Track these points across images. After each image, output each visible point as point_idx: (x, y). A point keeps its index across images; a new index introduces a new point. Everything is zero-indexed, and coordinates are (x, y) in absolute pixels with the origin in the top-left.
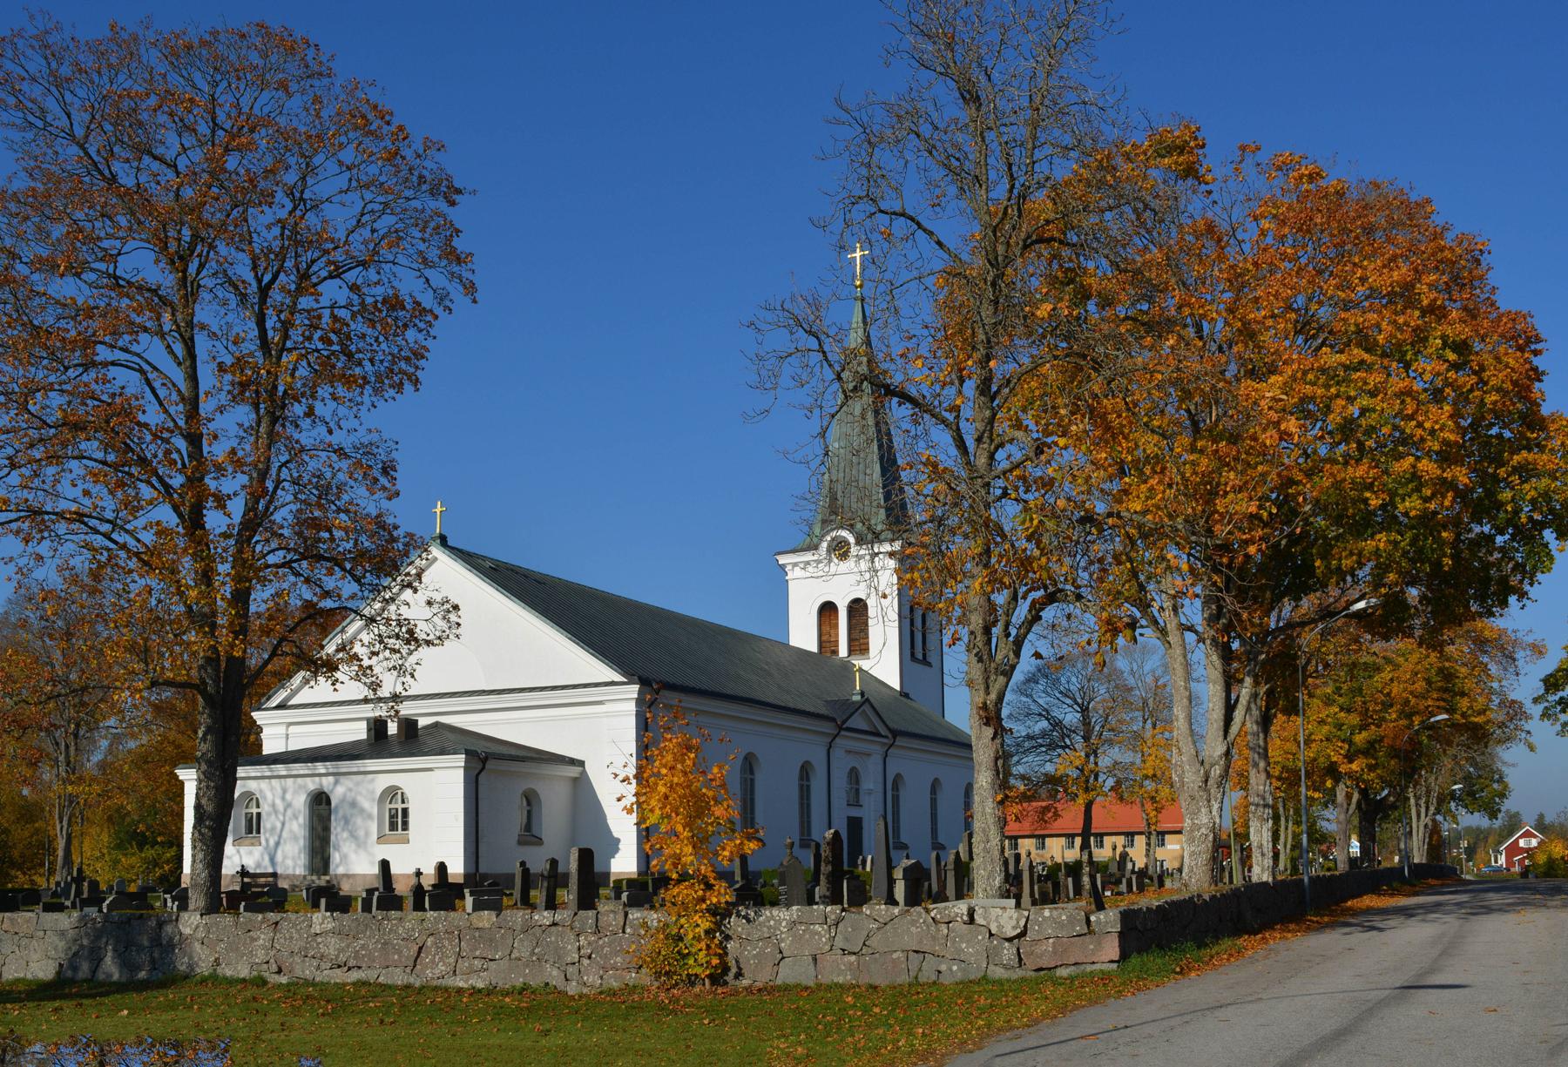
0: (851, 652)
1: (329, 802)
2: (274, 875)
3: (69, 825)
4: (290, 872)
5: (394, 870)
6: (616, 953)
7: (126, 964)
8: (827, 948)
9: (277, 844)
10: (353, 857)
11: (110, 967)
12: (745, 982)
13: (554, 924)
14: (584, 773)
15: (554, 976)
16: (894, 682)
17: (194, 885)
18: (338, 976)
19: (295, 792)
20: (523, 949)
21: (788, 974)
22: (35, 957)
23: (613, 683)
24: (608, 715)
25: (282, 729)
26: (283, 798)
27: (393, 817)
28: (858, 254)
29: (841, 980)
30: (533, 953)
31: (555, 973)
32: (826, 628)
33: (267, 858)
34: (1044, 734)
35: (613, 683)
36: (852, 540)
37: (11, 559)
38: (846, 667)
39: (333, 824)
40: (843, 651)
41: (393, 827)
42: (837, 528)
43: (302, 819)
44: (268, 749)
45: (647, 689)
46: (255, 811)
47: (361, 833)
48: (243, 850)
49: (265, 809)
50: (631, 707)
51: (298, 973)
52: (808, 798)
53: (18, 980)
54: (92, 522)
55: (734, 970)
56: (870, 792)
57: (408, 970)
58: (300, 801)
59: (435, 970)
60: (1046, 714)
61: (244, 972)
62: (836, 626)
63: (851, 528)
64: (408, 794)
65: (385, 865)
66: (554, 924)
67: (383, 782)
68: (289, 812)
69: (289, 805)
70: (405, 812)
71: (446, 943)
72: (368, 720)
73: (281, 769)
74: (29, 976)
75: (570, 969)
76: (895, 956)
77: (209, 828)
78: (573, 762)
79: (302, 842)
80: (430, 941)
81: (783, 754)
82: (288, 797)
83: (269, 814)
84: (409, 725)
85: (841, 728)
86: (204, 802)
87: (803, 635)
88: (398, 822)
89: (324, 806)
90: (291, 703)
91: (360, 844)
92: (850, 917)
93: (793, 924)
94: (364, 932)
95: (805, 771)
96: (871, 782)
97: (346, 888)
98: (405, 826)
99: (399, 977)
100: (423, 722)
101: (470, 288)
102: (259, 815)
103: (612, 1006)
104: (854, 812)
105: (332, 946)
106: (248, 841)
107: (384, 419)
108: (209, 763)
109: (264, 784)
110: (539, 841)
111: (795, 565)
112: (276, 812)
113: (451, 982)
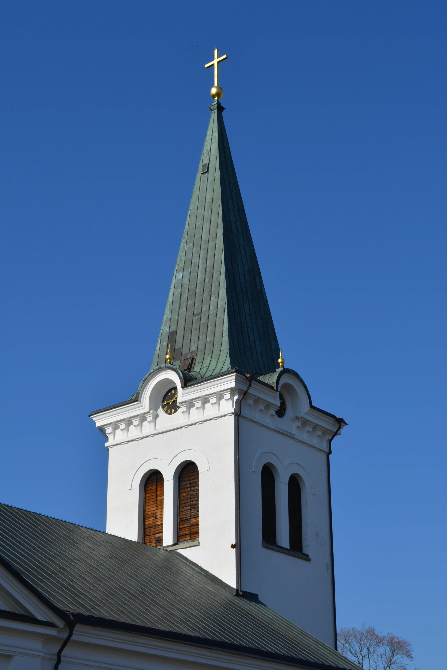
0: (179, 537)
36: (178, 383)
38: (174, 561)
40: (168, 538)
42: (160, 370)
111: (115, 426)
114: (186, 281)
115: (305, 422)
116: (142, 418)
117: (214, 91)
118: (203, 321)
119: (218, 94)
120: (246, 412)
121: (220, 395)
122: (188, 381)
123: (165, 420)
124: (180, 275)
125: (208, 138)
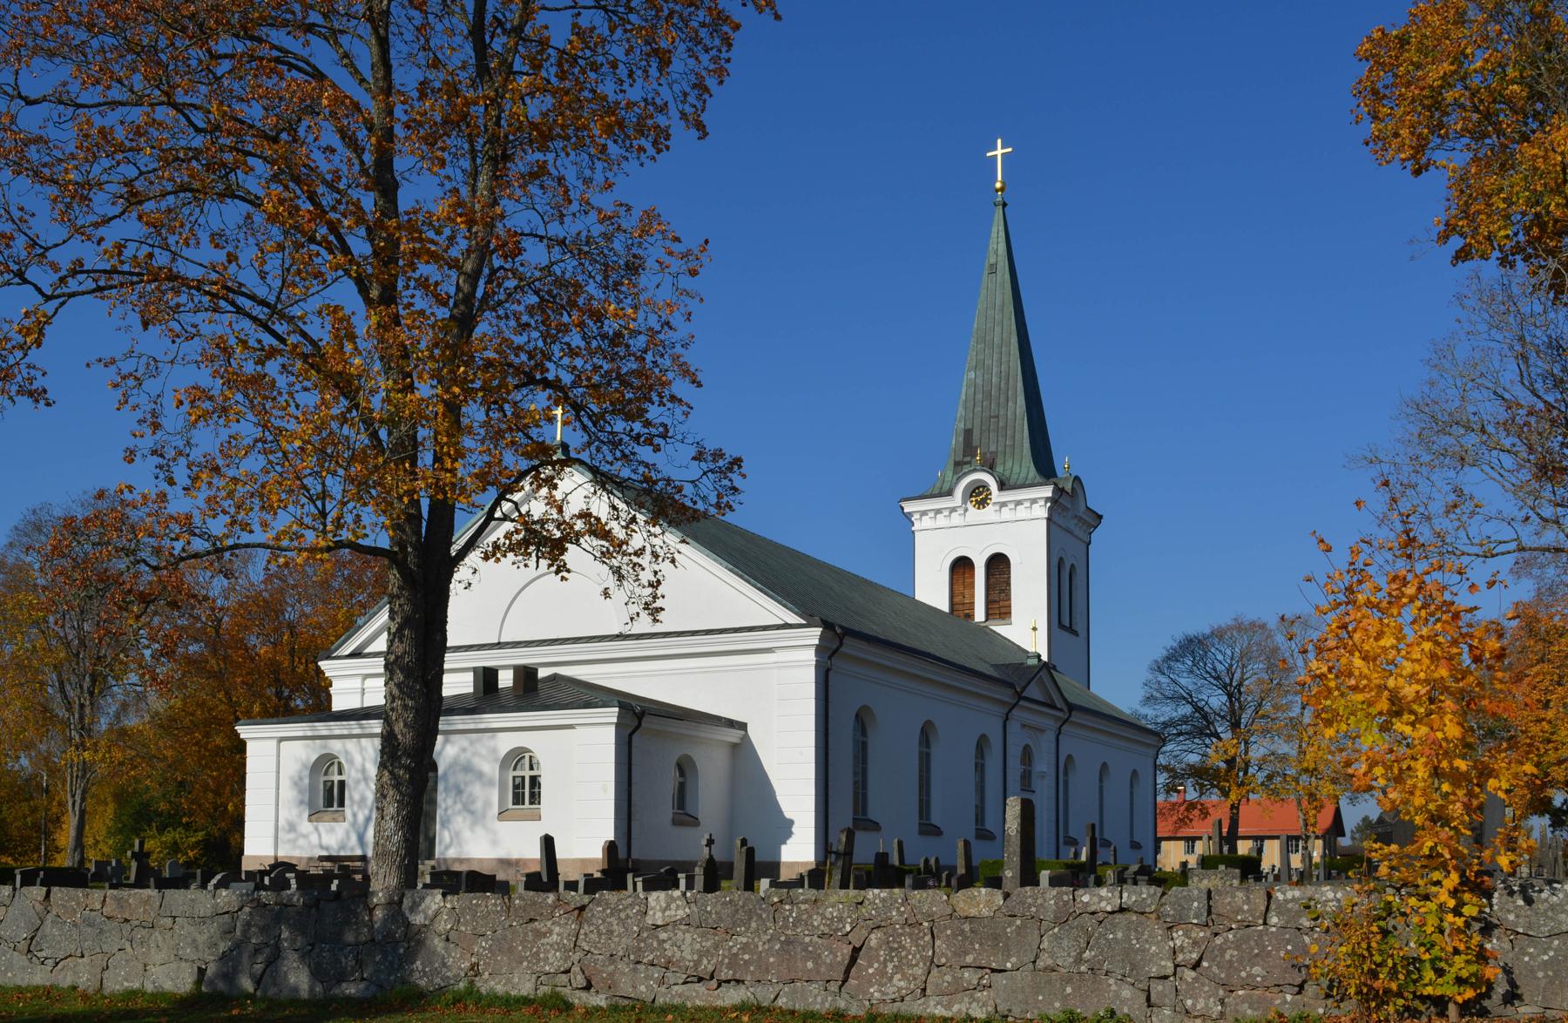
0: (988, 616)
3: (83, 799)
5: (560, 854)
10: (467, 834)
13: (1122, 910)
14: (746, 738)
17: (381, 854)
18: (699, 996)
20: (1059, 951)
22: (158, 957)
23: (787, 626)
24: (781, 666)
25: (357, 683)
27: (518, 787)
28: (999, 152)
30: (1079, 960)
31: (1126, 993)
32: (959, 588)
33: (354, 838)
34: (1184, 720)
35: (787, 626)
37: (113, 361)
40: (979, 615)
41: (518, 799)
42: (975, 470)
44: (337, 705)
45: (830, 633)
47: (479, 805)
48: (322, 826)
50: (810, 656)
52: (856, 795)
53: (132, 994)
54: (241, 301)
55: (1501, 989)
56: (1043, 776)
57: (833, 987)
60: (1188, 699)
61: (524, 986)
63: (990, 467)
64: (539, 755)
65: (548, 843)
66: (1122, 910)
67: (506, 743)
70: (535, 781)
71: (907, 942)
72: (475, 670)
74: (149, 988)
75: (1157, 987)
77: (407, 768)
78: (731, 724)
80: (874, 939)
81: (963, 723)
83: (358, 782)
84: (526, 675)
85: (1020, 697)
87: (932, 590)
88: (526, 793)
90: (367, 651)
91: (476, 817)
95: (982, 745)
96: (1043, 765)
98: (535, 798)
100: (543, 673)
102: (342, 784)
105: (686, 947)
106: (327, 816)
109: (351, 745)
110: (694, 821)
111: (924, 513)
113: (915, 1007)
114: (979, 381)
115: (1080, 519)
116: (953, 510)
117: (998, 185)
118: (1001, 424)
119: (1002, 189)
120: (1055, 518)
121: (1034, 501)
122: (1003, 486)
124: (972, 375)
125: (994, 235)
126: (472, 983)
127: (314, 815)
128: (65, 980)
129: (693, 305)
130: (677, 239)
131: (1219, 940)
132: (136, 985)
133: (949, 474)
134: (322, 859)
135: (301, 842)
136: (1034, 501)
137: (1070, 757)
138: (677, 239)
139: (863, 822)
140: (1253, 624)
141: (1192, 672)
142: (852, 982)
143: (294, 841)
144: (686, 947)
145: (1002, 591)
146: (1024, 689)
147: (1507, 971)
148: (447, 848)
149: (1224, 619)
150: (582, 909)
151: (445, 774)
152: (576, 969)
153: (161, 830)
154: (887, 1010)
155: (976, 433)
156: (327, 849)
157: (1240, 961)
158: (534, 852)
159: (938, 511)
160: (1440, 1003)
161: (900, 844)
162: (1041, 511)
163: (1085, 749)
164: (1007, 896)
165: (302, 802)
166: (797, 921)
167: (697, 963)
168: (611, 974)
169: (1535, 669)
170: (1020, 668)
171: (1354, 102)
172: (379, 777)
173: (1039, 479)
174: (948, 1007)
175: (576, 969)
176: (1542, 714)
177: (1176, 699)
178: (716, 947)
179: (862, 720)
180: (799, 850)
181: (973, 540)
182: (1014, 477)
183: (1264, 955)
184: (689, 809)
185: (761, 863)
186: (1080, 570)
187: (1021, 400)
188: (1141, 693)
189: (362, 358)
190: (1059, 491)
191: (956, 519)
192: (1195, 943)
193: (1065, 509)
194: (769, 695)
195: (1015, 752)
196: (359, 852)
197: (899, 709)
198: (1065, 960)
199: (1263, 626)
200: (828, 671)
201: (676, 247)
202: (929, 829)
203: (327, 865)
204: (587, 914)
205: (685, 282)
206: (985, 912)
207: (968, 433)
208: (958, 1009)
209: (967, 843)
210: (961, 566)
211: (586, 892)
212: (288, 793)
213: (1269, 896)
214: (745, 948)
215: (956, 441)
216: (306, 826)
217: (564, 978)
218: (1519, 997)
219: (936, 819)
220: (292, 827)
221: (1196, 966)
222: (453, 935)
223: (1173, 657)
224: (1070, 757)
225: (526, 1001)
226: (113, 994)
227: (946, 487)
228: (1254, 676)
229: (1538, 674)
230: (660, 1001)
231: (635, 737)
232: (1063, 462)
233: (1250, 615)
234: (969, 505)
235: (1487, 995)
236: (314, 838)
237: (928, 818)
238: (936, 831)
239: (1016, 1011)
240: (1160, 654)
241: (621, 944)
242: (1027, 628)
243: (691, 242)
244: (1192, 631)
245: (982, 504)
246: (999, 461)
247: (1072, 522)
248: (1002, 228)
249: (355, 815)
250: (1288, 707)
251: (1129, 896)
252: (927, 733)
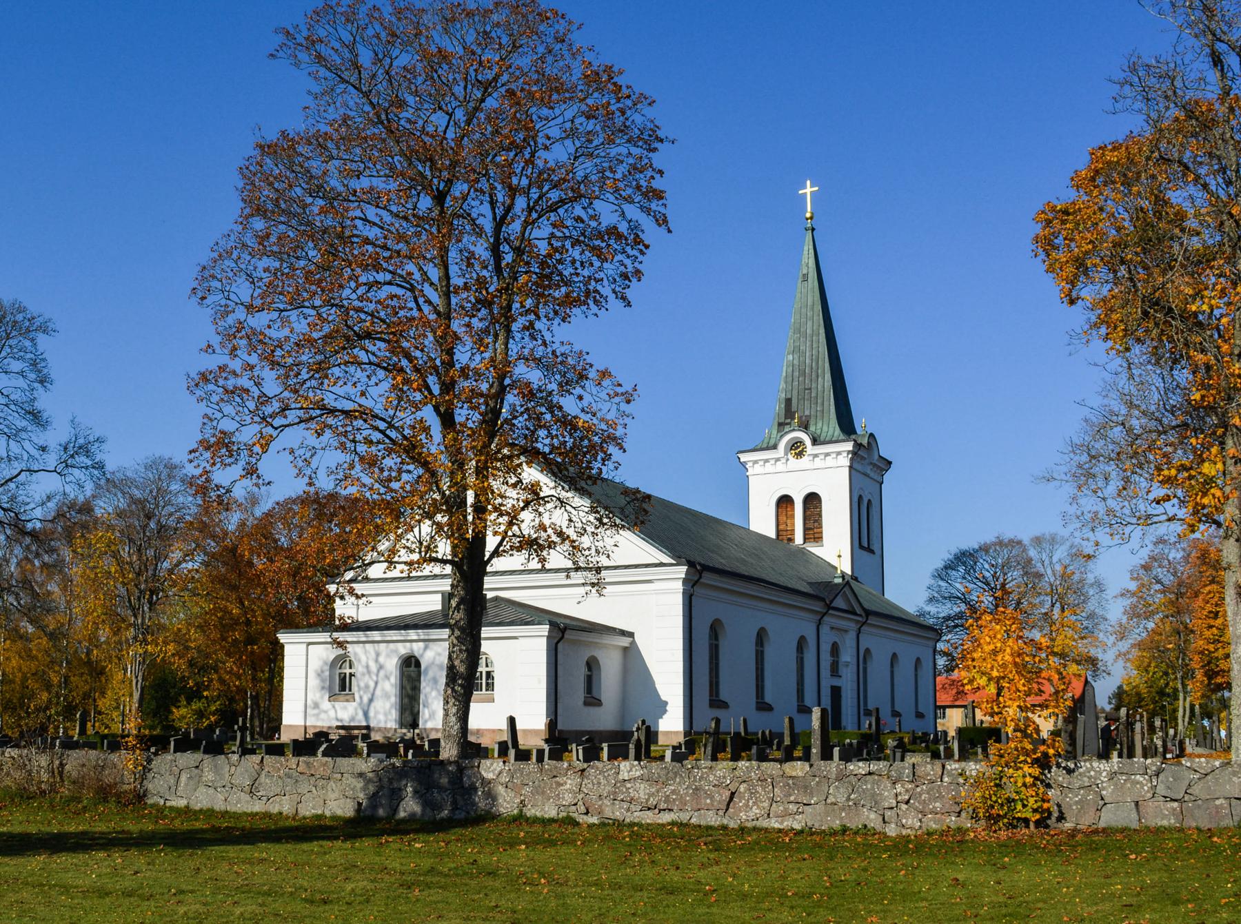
1: (418, 664)
2: (368, 728)
4: (382, 725)
5: (519, 726)
6: (936, 799)
7: (427, 803)
8: (1149, 795)
9: (371, 701)
11: (410, 806)
12: (1068, 825)
13: (870, 774)
14: (633, 643)
15: (872, 819)
16: (845, 566)
18: (649, 818)
19: (388, 656)
20: (838, 794)
21: (1108, 818)
22: (332, 796)
26: (377, 661)
29: (1165, 823)
30: (848, 799)
31: (873, 816)
39: (423, 684)
40: (799, 538)
41: (343, 688)
43: (394, 679)
45: (693, 570)
46: (348, 671)
48: (337, 705)
49: (359, 669)
50: (679, 586)
51: (608, 813)
53: (319, 817)
55: (1056, 815)
56: (847, 664)
57: (721, 813)
58: (392, 664)
59: (748, 813)
61: (551, 812)
62: (793, 516)
63: (805, 426)
66: (870, 774)
68: (382, 673)
69: (381, 667)
73: (376, 635)
75: (888, 813)
76: (1218, 802)
78: (623, 633)
79: (393, 699)
80: (742, 788)
81: (786, 629)
82: (381, 659)
83: (363, 674)
86: (457, 663)
87: (763, 522)
89: (413, 668)
92: (1170, 769)
93: (1112, 776)
94: (674, 779)
95: (801, 644)
96: (847, 656)
97: (485, 742)
99: (712, 819)
101: (662, 221)
103: (949, 845)
104: (836, 682)
105: (642, 791)
106: (341, 698)
107: (574, 333)
108: (462, 629)
110: (598, 703)
111: (756, 462)
112: (369, 672)
113: (764, 823)
114: (796, 362)
115: (875, 465)
116: (778, 460)
117: (808, 215)
119: (811, 218)
120: (856, 465)
121: (839, 453)
122: (815, 441)
123: (794, 463)
124: (790, 357)
125: (806, 252)
126: (521, 811)
127: (333, 697)
128: (274, 809)
129: (627, 420)
130: (620, 385)
131: (918, 789)
132: (320, 812)
133: (775, 432)
134: (338, 727)
135: (323, 716)
136: (839, 453)
137: (867, 651)
138: (620, 385)
139: (717, 702)
140: (1011, 541)
141: (964, 578)
142: (731, 810)
143: (317, 715)
144: (642, 791)
145: (815, 521)
146: (832, 602)
147: (1059, 806)
148: (426, 721)
149: (989, 538)
150: (583, 771)
151: (426, 669)
152: (580, 803)
153: (189, 701)
154: (749, 825)
155: (794, 402)
156: (342, 721)
157: (930, 799)
158: (504, 725)
159: (766, 461)
160: (1026, 821)
161: (745, 721)
162: (845, 461)
163: (880, 644)
164: (811, 766)
165: (323, 688)
166: (701, 778)
167: (648, 800)
168: (600, 806)
169: (1208, 588)
170: (829, 585)
171: (1034, 247)
172: (446, 691)
173: (842, 437)
174: (781, 823)
175: (580, 803)
176: (1212, 622)
177: (951, 598)
178: (658, 792)
179: (715, 629)
180: (672, 724)
181: (789, 484)
182: (823, 435)
183: (941, 797)
184: (595, 694)
185: (525, 731)
186: (875, 503)
187: (828, 376)
188: (926, 595)
189: (435, 442)
190: (858, 446)
191: (780, 466)
192: (907, 791)
193: (863, 458)
194: (647, 608)
195: (826, 648)
196: (364, 724)
197: (742, 621)
198: (841, 799)
199: (1019, 543)
200: (691, 596)
201: (619, 390)
202: (763, 706)
203: (342, 732)
204: (586, 773)
205: (623, 406)
206: (800, 774)
207: (788, 402)
208: (786, 824)
209: (791, 720)
210: (785, 502)
211: (585, 761)
212: (314, 682)
213: (943, 767)
214: (673, 792)
215: (778, 408)
216: (326, 704)
217: (574, 808)
218: (1065, 819)
219: (768, 698)
220: (316, 706)
221: (907, 802)
222: (510, 785)
223: (949, 567)
224: (867, 651)
225: (552, 820)
226: (304, 818)
227: (772, 442)
228: (1014, 578)
229: (1210, 592)
230: (628, 820)
231: (560, 645)
232: (861, 422)
233: (1008, 535)
234: (790, 456)
235: (1049, 817)
236: (332, 713)
237: (763, 698)
238: (769, 708)
239: (817, 825)
240: (940, 564)
241: (605, 790)
242: (835, 549)
243: (627, 387)
244: (965, 546)
245: (800, 455)
246: (812, 422)
247: (869, 465)
248: (811, 247)
249: (361, 698)
250: (1042, 603)
251: (874, 766)
252: (761, 637)
